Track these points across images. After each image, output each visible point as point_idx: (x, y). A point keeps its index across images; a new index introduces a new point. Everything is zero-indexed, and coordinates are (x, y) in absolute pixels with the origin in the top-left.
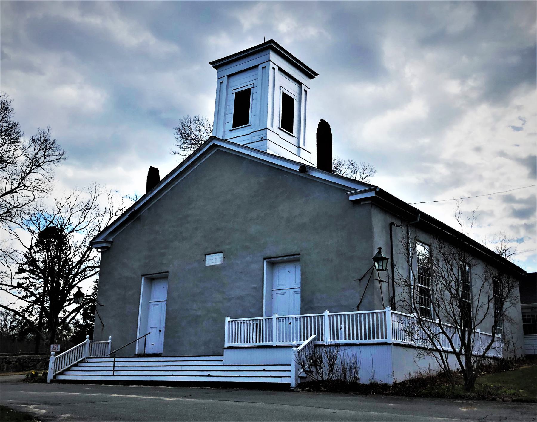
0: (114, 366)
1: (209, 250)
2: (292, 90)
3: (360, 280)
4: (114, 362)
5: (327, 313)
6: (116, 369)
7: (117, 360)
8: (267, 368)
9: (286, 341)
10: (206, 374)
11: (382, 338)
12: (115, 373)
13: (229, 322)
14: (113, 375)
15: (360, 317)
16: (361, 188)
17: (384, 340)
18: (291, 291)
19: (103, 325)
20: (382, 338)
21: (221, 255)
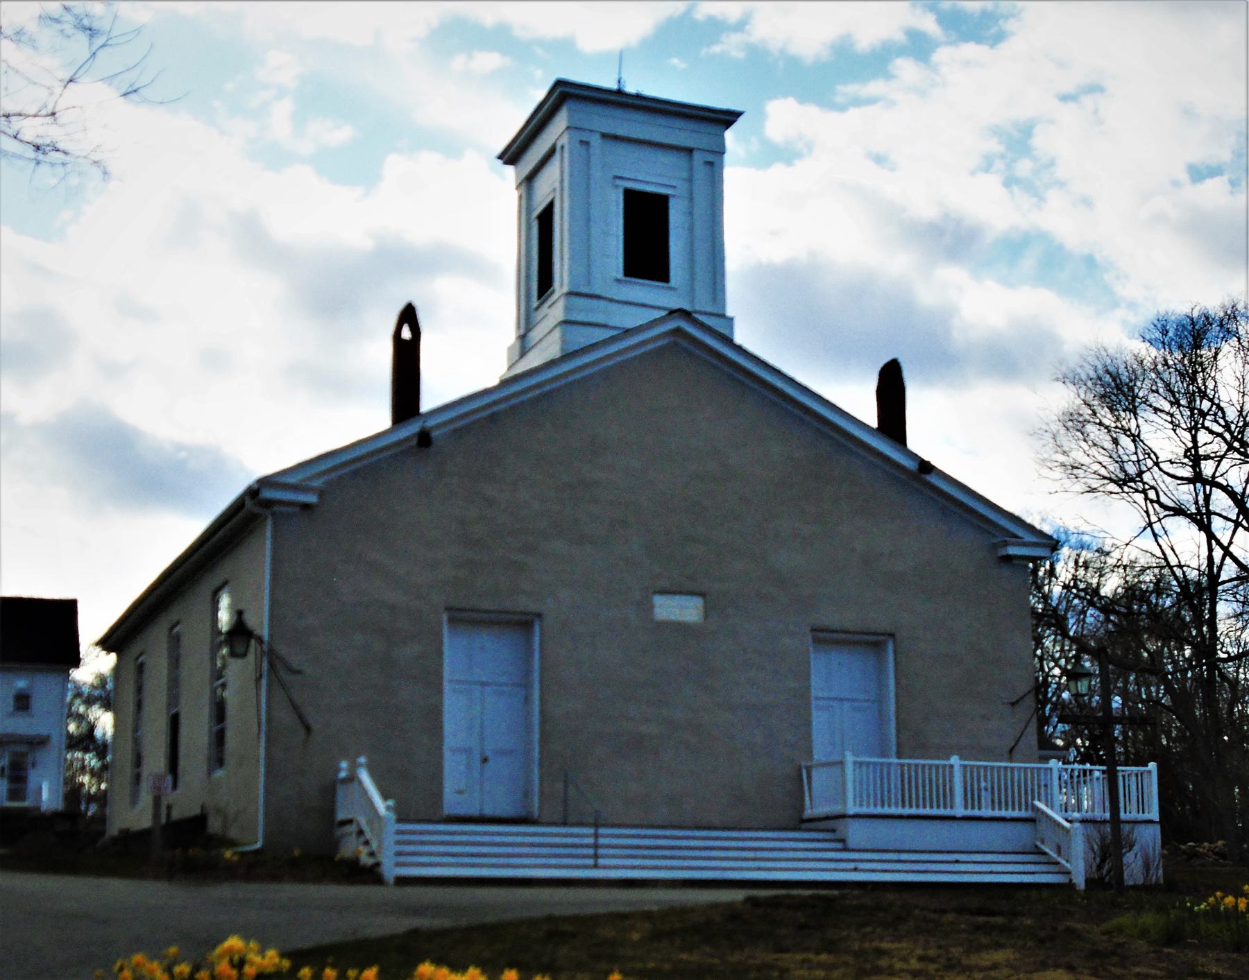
0: (596, 846)
1: (664, 583)
2: (653, 174)
3: (1013, 704)
4: (596, 836)
5: (954, 760)
6: (601, 851)
7: (601, 831)
8: (904, 856)
9: (868, 806)
10: (852, 865)
11: (918, 806)
12: (601, 861)
13: (855, 763)
14: (596, 866)
15: (999, 772)
16: (1029, 538)
17: (948, 812)
18: (846, 705)
19: (308, 729)
20: (945, 807)
21: (697, 602)
